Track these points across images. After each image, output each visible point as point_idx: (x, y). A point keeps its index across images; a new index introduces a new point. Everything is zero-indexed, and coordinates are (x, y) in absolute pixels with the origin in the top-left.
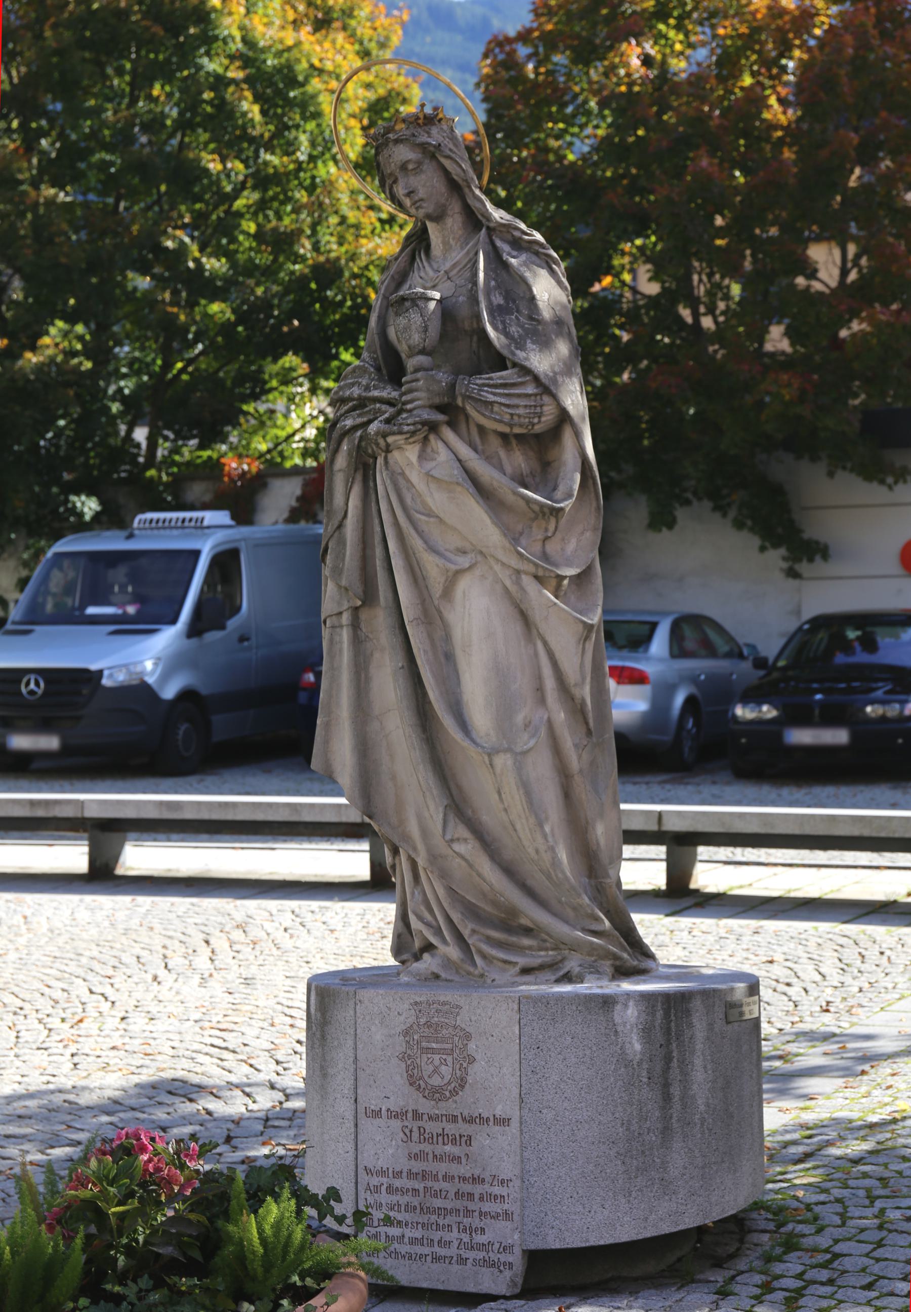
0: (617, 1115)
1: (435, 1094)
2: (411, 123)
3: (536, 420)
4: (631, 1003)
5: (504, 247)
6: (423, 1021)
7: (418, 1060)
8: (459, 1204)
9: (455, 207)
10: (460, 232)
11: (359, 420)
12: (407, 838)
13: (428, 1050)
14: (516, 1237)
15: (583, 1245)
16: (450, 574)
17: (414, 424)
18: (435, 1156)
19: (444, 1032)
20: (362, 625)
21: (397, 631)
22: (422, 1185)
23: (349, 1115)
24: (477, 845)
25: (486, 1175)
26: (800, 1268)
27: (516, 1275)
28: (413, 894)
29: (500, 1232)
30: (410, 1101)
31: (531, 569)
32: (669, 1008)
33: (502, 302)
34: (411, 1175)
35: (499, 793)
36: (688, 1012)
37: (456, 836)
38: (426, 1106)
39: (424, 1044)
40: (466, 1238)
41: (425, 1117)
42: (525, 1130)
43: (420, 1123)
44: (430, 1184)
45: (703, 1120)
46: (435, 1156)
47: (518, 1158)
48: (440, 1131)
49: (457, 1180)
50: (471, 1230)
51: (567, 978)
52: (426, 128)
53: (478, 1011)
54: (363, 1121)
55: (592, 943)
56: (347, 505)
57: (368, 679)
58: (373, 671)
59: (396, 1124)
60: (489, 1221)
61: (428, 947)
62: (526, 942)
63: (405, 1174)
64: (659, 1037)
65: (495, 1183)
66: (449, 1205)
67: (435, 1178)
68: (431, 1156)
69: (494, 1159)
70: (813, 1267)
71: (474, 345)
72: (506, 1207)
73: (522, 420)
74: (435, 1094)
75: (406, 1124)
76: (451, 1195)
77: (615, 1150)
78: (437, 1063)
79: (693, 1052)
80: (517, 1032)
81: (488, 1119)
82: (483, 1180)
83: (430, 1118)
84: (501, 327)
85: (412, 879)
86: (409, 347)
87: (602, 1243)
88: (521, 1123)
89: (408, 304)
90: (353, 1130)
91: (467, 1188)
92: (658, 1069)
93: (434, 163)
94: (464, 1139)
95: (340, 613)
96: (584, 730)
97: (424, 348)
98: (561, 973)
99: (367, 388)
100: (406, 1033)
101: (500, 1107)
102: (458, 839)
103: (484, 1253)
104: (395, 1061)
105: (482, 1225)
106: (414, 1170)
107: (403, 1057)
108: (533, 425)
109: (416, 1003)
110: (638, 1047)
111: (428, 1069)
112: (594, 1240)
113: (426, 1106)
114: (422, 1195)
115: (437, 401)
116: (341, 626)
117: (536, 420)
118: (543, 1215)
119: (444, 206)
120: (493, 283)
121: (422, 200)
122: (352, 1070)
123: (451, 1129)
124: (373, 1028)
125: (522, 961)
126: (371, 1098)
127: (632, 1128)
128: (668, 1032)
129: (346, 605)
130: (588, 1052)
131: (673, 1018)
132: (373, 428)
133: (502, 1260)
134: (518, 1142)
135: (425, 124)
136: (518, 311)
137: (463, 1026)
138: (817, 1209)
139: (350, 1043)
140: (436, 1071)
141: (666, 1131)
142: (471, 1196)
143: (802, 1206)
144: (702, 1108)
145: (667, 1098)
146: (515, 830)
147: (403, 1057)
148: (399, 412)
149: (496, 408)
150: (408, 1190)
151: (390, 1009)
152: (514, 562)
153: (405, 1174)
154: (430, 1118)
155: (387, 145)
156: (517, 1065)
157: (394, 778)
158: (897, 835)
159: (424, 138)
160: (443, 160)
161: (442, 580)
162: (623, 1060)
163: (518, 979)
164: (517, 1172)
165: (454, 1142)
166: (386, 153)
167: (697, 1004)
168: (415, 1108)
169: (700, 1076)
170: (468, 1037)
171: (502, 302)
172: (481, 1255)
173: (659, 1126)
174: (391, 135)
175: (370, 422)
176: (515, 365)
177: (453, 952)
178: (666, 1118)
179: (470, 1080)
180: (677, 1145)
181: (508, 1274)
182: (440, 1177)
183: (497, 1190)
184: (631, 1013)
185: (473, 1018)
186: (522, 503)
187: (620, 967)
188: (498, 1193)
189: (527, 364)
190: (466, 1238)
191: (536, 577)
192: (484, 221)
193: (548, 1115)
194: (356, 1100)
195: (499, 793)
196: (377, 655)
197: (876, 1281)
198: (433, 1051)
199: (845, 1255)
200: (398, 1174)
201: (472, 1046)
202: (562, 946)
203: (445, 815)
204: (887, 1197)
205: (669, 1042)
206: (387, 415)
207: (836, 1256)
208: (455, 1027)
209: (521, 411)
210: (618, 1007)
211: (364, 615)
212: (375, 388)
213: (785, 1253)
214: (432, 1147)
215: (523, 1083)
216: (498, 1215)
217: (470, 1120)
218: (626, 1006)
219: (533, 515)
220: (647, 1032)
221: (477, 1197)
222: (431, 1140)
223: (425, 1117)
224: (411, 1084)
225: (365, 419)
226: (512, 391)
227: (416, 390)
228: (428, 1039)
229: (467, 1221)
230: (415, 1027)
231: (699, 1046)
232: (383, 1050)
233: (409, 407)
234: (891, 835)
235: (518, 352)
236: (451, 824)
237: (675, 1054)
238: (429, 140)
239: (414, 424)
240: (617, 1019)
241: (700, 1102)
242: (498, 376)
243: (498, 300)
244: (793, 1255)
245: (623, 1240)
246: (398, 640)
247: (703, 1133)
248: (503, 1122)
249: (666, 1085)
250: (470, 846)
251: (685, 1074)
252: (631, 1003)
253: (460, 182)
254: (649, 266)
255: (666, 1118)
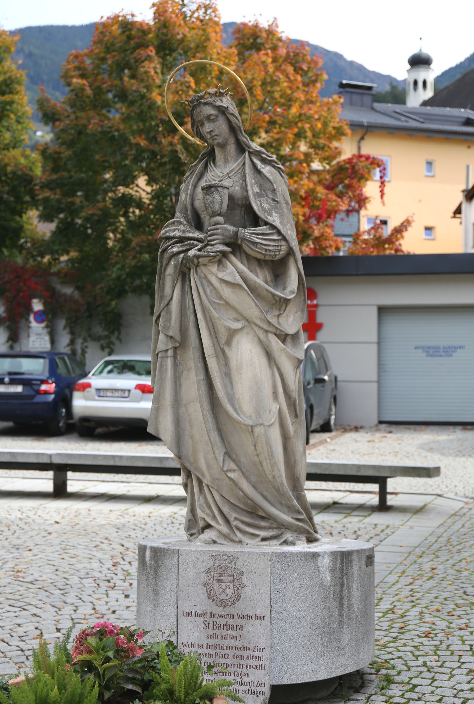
0: (319, 614)
1: (223, 604)
2: (213, 95)
3: (277, 253)
4: (326, 556)
5: (259, 164)
6: (216, 565)
7: (214, 586)
8: (235, 661)
9: (232, 141)
10: (234, 153)
11: (181, 249)
12: (198, 469)
13: (219, 580)
14: (267, 678)
15: (302, 682)
16: (231, 331)
17: (215, 252)
18: (222, 636)
19: (229, 571)
20: (178, 357)
21: (201, 360)
22: (214, 652)
23: (173, 615)
24: (240, 473)
25: (251, 646)
26: (401, 693)
27: (266, 698)
28: (199, 499)
29: (257, 676)
30: (209, 607)
31: (274, 330)
32: (343, 559)
33: (258, 191)
34: (208, 646)
35: (255, 446)
36: (351, 561)
37: (229, 468)
38: (217, 610)
39: (217, 577)
40: (239, 679)
41: (217, 616)
42: (273, 622)
43: (214, 619)
44: (218, 651)
45: (357, 616)
46: (222, 636)
47: (269, 637)
48: (225, 623)
49: (234, 649)
50: (241, 675)
51: (286, 543)
52: (220, 98)
53: (248, 560)
54: (181, 618)
55: (298, 525)
56: (173, 293)
57: (180, 385)
58: (183, 381)
59: (200, 620)
60: (251, 670)
61: (208, 526)
62: (263, 524)
63: (204, 646)
64: (338, 574)
65: (256, 650)
66: (229, 662)
67: (222, 648)
68: (219, 636)
69: (255, 638)
70: (407, 691)
71: (243, 213)
72: (261, 662)
73: (271, 253)
74: (223, 604)
75: (206, 619)
76: (231, 657)
77: (317, 632)
78: (224, 587)
79: (353, 582)
80: (270, 571)
81: (252, 617)
82: (249, 649)
83: (220, 616)
84: (259, 204)
85: (198, 491)
86: (213, 212)
87: (310, 681)
88: (271, 619)
89: (213, 189)
90: (175, 623)
91: (239, 653)
92: (338, 590)
93: (224, 117)
94: (238, 627)
95: (167, 350)
96: (294, 414)
97: (220, 213)
98: (283, 540)
99: (184, 232)
100: (207, 572)
101: (259, 610)
102: (230, 470)
103: (249, 687)
104: (200, 586)
105: (248, 672)
106: (210, 644)
107: (205, 584)
108: (276, 255)
109: (213, 556)
110: (329, 579)
111: (219, 591)
112: (307, 679)
113: (217, 610)
114: (214, 657)
115: (227, 240)
116: (167, 357)
117: (277, 253)
118: (281, 667)
119: (227, 139)
120: (253, 181)
121: (216, 135)
122: (176, 591)
123: (231, 622)
124: (188, 569)
125: (263, 534)
126: (186, 606)
127: (326, 621)
128: (342, 571)
129: (170, 346)
130: (305, 581)
131: (345, 564)
132: (192, 252)
133: (259, 691)
134: (269, 628)
135: (220, 96)
136: (267, 196)
137: (239, 568)
138: (392, 662)
139: (175, 576)
140: (223, 591)
141: (341, 622)
142: (242, 657)
143: (383, 661)
144: (356, 610)
145: (341, 605)
146: (262, 466)
147: (205, 584)
148: (206, 246)
149: (259, 246)
150: (206, 654)
151: (198, 559)
152: (265, 326)
153: (204, 646)
154: (220, 616)
155: (199, 106)
156: (269, 588)
157: (192, 437)
158: (334, 473)
159: (219, 103)
160: (228, 115)
161: (227, 334)
162: (322, 586)
163: (260, 543)
164: (268, 644)
165: (233, 628)
166: (198, 109)
167: (355, 557)
168: (211, 611)
169: (355, 594)
170: (242, 573)
171: (258, 191)
172: (247, 688)
173: (338, 619)
174: (202, 100)
175: (190, 249)
176: (266, 223)
177: (224, 529)
178: (341, 616)
179: (242, 596)
180: (346, 629)
181: (262, 697)
182: (225, 647)
183: (256, 654)
184: (325, 562)
185: (245, 564)
186: (270, 296)
187: (309, 537)
188: (257, 655)
189: (274, 223)
190: (239, 679)
191: (276, 334)
192: (247, 148)
193: (285, 614)
194: (177, 607)
195: (255, 446)
196: (185, 373)
197: (442, 698)
198: (222, 581)
199: (418, 685)
200: (201, 646)
201: (244, 578)
202: (282, 527)
203: (224, 458)
204: (423, 656)
205: (343, 577)
206: (199, 247)
207: (415, 686)
208: (235, 568)
209: (271, 248)
210: (320, 558)
211: (178, 352)
212: (189, 232)
213: (388, 685)
214: (220, 631)
215: (272, 598)
216: (257, 667)
217: (243, 617)
218: (324, 557)
219: (274, 302)
220: (333, 571)
221: (245, 657)
222: (220, 627)
223: (217, 616)
224: (209, 599)
225: (184, 248)
226: (267, 237)
227: (216, 234)
228: (219, 575)
229: (239, 670)
230: (212, 568)
231: (355, 578)
232: (193, 580)
233: (212, 243)
234: (331, 473)
235: (269, 217)
236: (227, 462)
237: (345, 583)
238: (222, 104)
239: (215, 252)
240: (320, 565)
241: (356, 607)
242: (259, 230)
243: (257, 190)
244: (393, 686)
245: (321, 679)
246: (200, 365)
247: (356, 623)
248: (261, 618)
249: (341, 599)
250: (236, 474)
251: (349, 593)
252: (326, 556)
253: (236, 127)
254: (146, 177)
255: (341, 616)
